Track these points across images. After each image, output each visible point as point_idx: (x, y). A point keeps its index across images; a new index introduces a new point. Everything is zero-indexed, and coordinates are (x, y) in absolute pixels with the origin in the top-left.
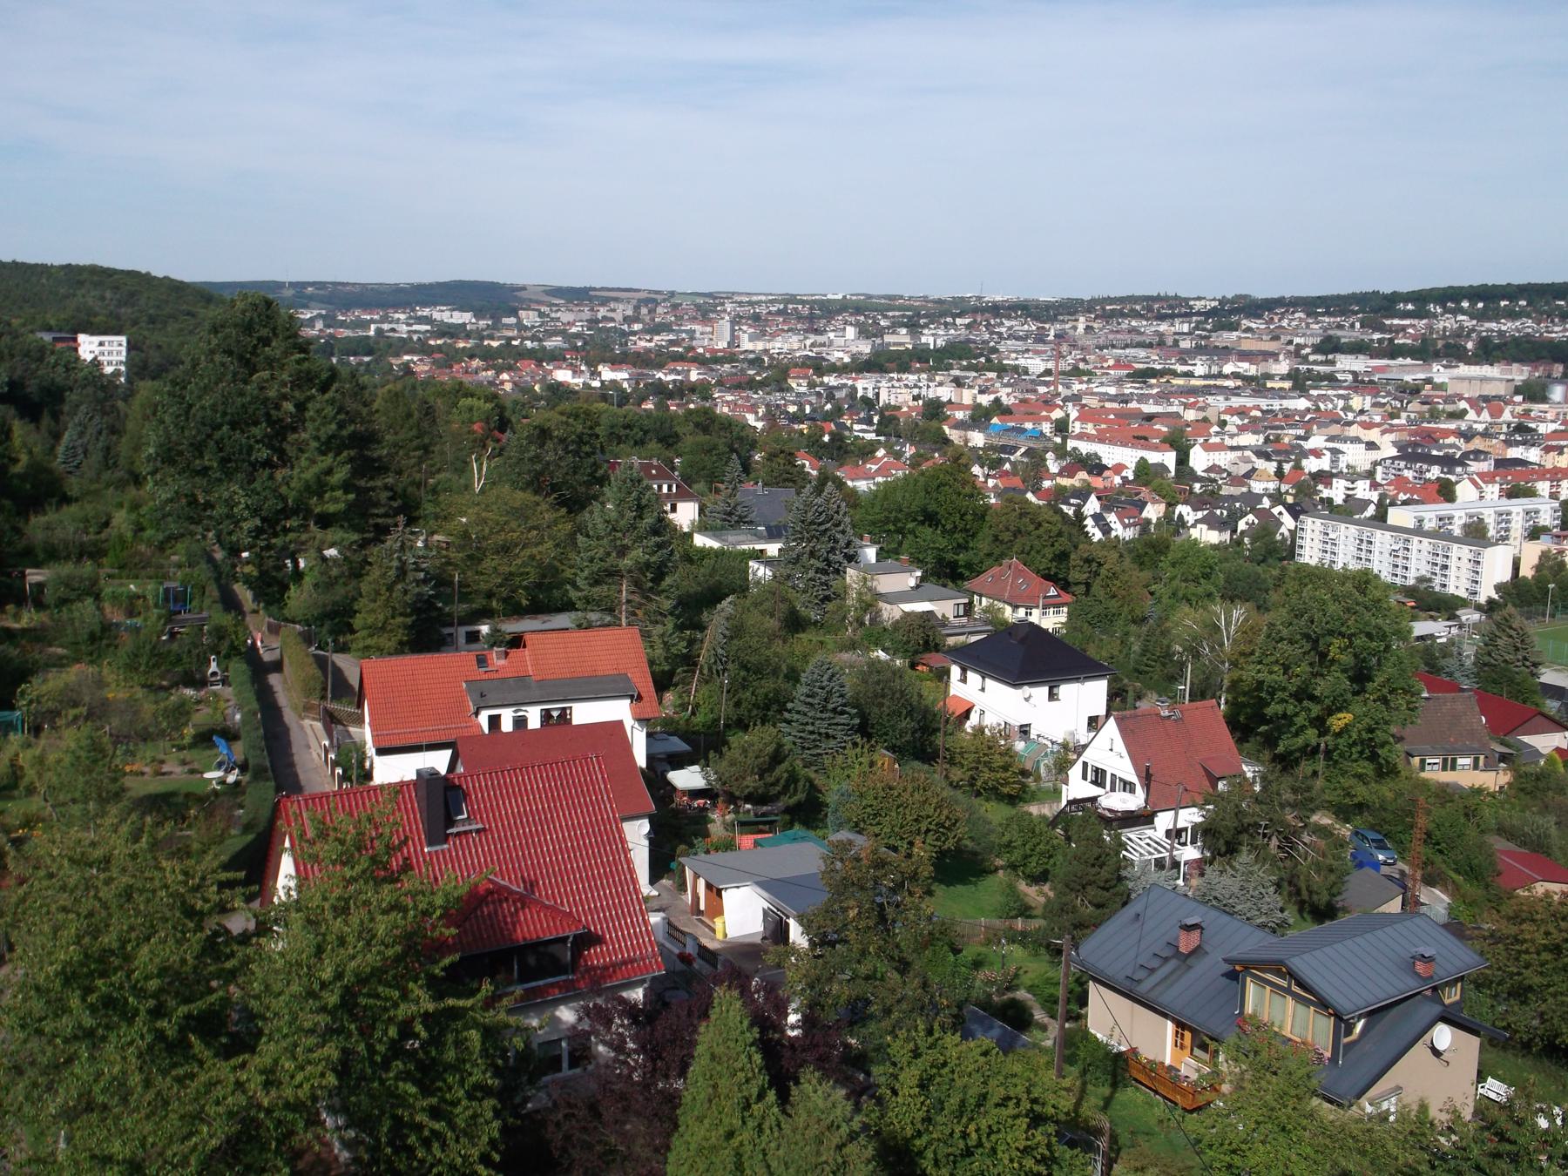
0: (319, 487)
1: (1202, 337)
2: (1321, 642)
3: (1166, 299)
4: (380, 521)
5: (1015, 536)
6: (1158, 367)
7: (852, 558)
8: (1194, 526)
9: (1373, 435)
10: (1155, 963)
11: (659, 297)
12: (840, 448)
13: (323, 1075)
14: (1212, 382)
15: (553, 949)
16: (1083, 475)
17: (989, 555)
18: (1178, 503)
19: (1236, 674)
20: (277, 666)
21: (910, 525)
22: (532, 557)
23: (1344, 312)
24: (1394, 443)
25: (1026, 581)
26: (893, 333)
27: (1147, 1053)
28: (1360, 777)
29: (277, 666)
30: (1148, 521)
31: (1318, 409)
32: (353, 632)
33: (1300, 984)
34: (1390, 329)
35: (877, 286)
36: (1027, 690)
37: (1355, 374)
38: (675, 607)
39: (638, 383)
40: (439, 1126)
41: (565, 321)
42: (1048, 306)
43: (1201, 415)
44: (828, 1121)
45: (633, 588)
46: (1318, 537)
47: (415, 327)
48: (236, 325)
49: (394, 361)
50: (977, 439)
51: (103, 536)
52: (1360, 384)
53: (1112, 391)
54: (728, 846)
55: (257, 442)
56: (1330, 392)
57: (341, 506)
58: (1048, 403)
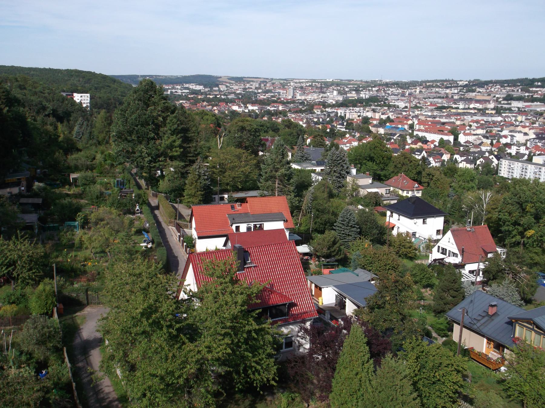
0: (171, 147)
1: (461, 95)
2: (523, 205)
3: (449, 81)
4: (191, 158)
5: (402, 166)
6: (446, 105)
7: (348, 173)
8: (461, 162)
9: (526, 130)
10: (479, 318)
11: (267, 81)
12: (333, 134)
13: (226, 349)
14: (466, 111)
15: (281, 308)
16: (420, 144)
17: (393, 172)
18: (454, 154)
19: (490, 215)
20: (157, 208)
21: (364, 161)
22: (242, 172)
23: (515, 86)
24: (534, 133)
25: (407, 181)
26: (351, 93)
27: (477, 349)
28: (536, 253)
29: (157, 208)
30: (444, 161)
31: (505, 121)
32: (184, 197)
33: (538, 327)
34: (532, 92)
35: (344, 76)
36: (415, 220)
37: (519, 108)
38: (295, 189)
39: (261, 111)
40: (259, 367)
41: (235, 88)
42: (406, 84)
43: (462, 123)
44: (397, 371)
45: (280, 183)
46: (507, 167)
47: (184, 91)
48: (142, 91)
49: (177, 103)
50: (382, 131)
51: (94, 162)
52: (520, 111)
53: (430, 114)
54: (319, 273)
55: (150, 131)
56: (510, 115)
57: (179, 153)
58: (406, 118)
